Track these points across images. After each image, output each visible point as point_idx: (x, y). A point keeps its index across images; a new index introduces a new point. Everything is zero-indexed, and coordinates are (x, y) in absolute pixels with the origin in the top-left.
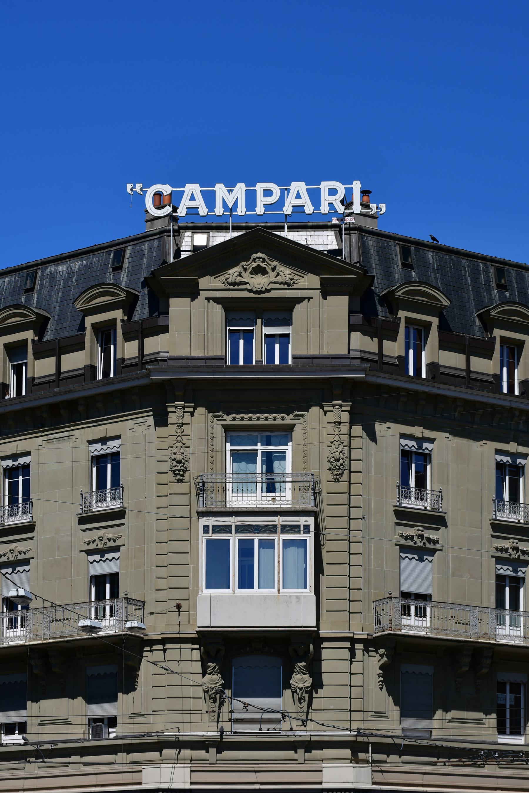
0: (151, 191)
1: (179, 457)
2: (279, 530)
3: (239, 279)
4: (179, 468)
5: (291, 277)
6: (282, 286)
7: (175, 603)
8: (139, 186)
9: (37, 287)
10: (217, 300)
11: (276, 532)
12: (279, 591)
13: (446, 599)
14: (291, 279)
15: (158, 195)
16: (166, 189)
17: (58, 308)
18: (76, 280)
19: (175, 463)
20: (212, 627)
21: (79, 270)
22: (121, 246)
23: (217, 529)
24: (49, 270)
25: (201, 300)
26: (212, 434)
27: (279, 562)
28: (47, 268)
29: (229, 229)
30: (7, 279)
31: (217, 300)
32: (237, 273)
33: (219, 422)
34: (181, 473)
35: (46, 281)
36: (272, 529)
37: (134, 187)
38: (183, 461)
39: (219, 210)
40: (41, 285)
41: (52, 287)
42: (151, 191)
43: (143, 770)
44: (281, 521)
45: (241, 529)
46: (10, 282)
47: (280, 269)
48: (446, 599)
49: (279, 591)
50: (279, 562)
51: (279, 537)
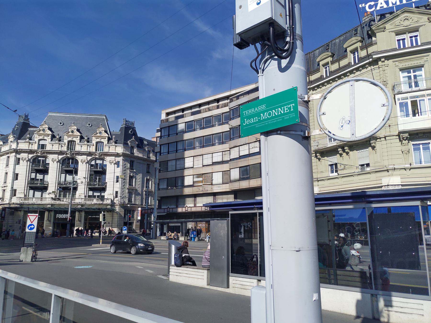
0: (367, 6)
1: (385, 80)
2: (426, 96)
3: (400, 24)
4: (385, 83)
5: (418, 20)
6: (415, 23)
7: (389, 125)
8: (363, 5)
9: (330, 48)
10: (392, 31)
11: (425, 96)
12: (428, 115)
13: (50, 184)
14: (418, 21)
15: (370, 5)
16: (372, 3)
17: (337, 51)
18: (342, 42)
19: (383, 82)
20: (404, 130)
21: (343, 39)
22: (356, 28)
23: (403, 99)
24: (333, 42)
25: (387, 31)
26: (396, 71)
27: (427, 106)
28: (333, 42)
29: (229, 218)
30: (320, 49)
31: (392, 31)
32: (399, 22)
33: (397, 68)
34: (386, 85)
35: (333, 45)
36: (424, 96)
37: (362, 5)
38: (386, 81)
39: (391, 5)
40: (331, 47)
41: (334, 46)
42: (367, 6)
43: (382, 179)
44: (426, 92)
45: (411, 97)
46: (321, 49)
47: (413, 18)
48: (50, 184)
49: (428, 115)
50: (427, 106)
51: (426, 98)
